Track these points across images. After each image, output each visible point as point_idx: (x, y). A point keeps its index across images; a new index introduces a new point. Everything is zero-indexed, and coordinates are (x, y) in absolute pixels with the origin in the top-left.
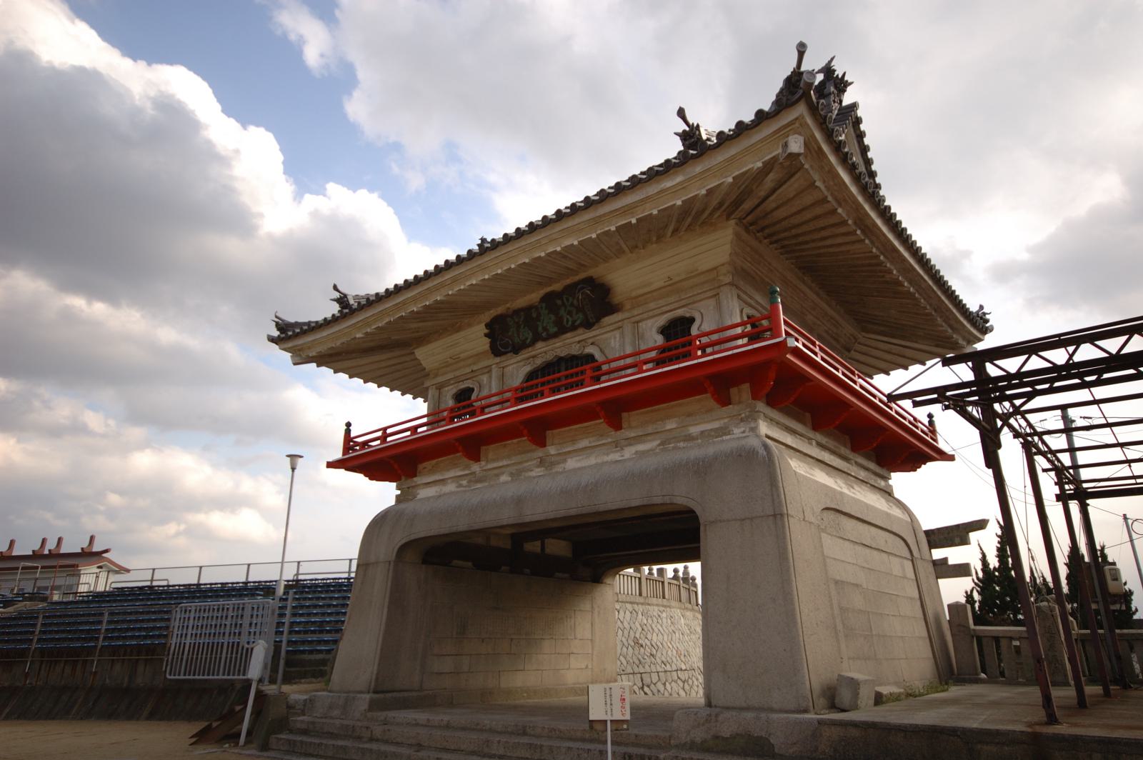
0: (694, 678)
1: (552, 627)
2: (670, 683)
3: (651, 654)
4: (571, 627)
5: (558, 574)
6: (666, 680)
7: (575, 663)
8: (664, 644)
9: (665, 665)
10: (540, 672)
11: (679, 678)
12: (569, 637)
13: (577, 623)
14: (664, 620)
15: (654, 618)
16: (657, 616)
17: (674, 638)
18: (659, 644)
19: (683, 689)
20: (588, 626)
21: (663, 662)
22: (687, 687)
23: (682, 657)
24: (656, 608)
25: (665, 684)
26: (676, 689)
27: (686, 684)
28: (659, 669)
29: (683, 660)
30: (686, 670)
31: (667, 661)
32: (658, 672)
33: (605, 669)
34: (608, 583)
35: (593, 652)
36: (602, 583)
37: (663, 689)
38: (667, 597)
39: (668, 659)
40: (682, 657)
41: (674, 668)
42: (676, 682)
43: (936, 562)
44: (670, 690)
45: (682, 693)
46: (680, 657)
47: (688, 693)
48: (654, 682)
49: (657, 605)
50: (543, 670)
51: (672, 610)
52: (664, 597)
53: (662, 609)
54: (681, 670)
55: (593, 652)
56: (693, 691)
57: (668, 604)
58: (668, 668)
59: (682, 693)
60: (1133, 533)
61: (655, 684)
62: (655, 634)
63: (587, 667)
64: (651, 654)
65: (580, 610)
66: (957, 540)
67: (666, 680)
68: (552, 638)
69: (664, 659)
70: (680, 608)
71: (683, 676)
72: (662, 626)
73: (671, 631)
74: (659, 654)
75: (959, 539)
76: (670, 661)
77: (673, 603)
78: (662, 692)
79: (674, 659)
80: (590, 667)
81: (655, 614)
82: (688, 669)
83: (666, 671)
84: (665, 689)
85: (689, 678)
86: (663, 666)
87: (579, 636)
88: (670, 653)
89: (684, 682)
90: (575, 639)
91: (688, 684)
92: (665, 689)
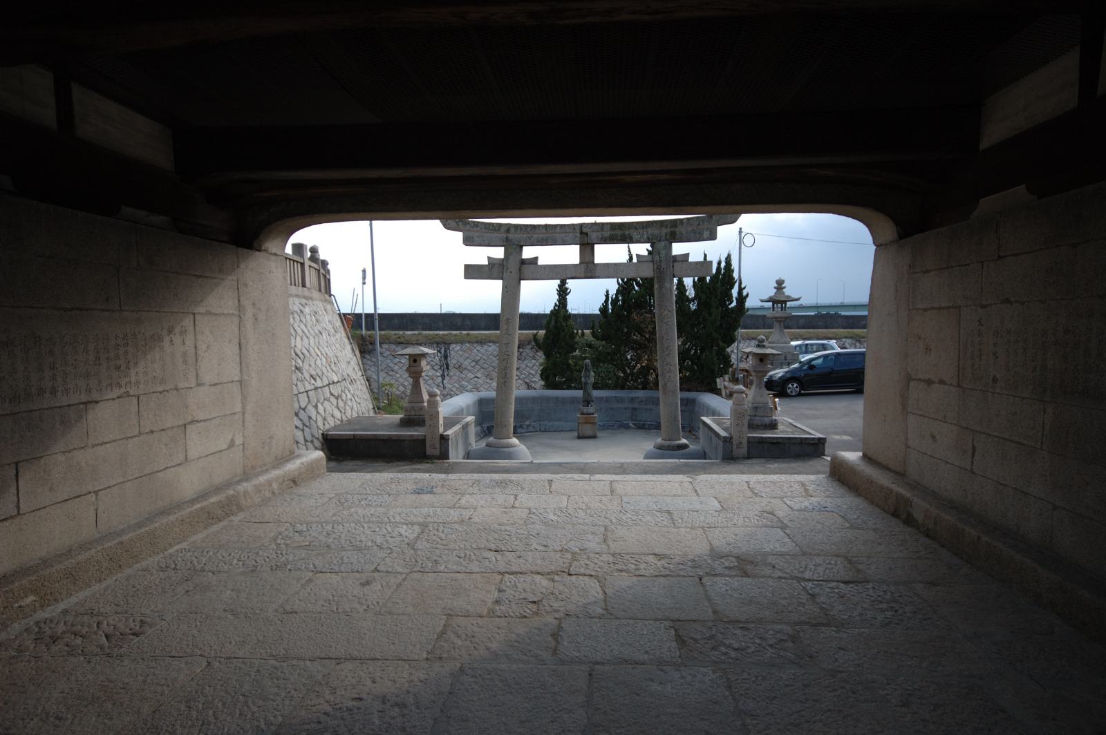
0: (346, 391)
1: (121, 362)
2: (322, 404)
3: (297, 368)
4: (185, 354)
5: (127, 210)
6: (318, 401)
7: (197, 443)
8: (311, 350)
9: (315, 380)
10: (92, 497)
11: (331, 394)
12: (181, 385)
13: (202, 347)
14: (308, 317)
15: (296, 315)
16: (299, 311)
17: (321, 341)
18: (305, 351)
19: (337, 407)
20: (231, 350)
21: (311, 376)
22: (341, 404)
23: (333, 366)
24: (297, 300)
25: (316, 407)
26: (330, 409)
27: (340, 400)
28: (309, 387)
29: (334, 369)
30: (338, 382)
31: (317, 374)
32: (307, 392)
33: (271, 437)
34: (274, 250)
35: (244, 408)
36: (259, 250)
37: (315, 413)
38: (308, 284)
39: (318, 370)
40: (333, 366)
41: (326, 382)
42: (329, 400)
43: (678, 259)
44: (323, 414)
45: (337, 414)
46: (330, 366)
47: (343, 411)
48: (303, 407)
49: (297, 296)
50: (96, 492)
51: (314, 302)
52: (304, 286)
53: (304, 301)
54: (334, 383)
55: (244, 408)
56: (348, 408)
57: (309, 296)
58: (319, 383)
59: (337, 414)
60: (743, 245)
61: (304, 409)
62: (298, 338)
63: (232, 444)
64: (297, 368)
65: (209, 313)
66: (706, 234)
67: (318, 401)
68: (128, 395)
69: (314, 373)
70: (321, 300)
71: (336, 390)
72: (306, 326)
73: (317, 332)
74: (306, 367)
75: (708, 232)
76: (320, 374)
77: (316, 294)
78: (314, 418)
79: (325, 371)
80: (239, 441)
81: (296, 308)
82: (340, 380)
83: (316, 389)
84: (318, 412)
85: (342, 391)
86: (313, 381)
87: (208, 378)
88: (318, 362)
89: (337, 398)
90: (198, 385)
91: (342, 400)
92: (318, 412)
